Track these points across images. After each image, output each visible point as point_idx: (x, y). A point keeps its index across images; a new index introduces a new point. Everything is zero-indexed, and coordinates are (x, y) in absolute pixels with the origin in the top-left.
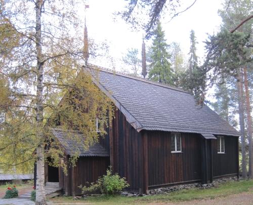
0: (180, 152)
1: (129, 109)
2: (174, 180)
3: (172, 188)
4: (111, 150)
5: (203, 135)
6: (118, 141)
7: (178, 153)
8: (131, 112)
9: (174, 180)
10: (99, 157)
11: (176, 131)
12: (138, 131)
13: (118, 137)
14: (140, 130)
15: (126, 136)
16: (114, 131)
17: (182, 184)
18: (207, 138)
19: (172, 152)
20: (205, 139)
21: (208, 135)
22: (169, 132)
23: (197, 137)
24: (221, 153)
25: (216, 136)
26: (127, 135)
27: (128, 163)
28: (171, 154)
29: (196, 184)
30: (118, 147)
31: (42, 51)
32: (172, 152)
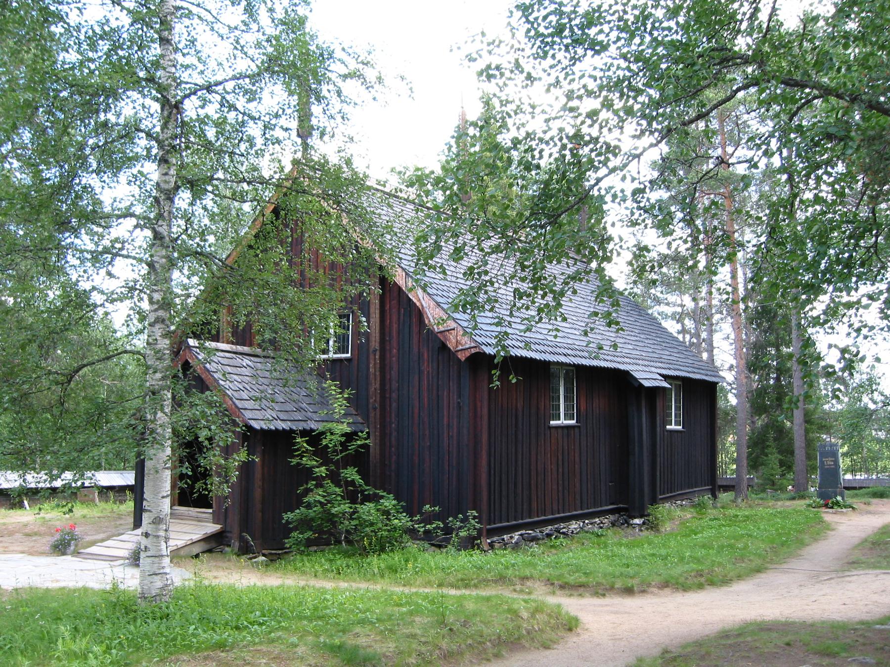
0: (573, 422)
1: (435, 292)
2: (555, 507)
3: (548, 529)
4: (372, 415)
5: (637, 375)
6: (395, 385)
7: (568, 427)
8: (439, 299)
9: (555, 507)
10: (269, 431)
11: (563, 359)
12: (462, 357)
13: (394, 374)
14: (468, 354)
15: (420, 372)
16: (383, 358)
17: (576, 518)
18: (646, 384)
19: (668, 427)
20: (641, 385)
21: (648, 375)
22: (546, 364)
23: (620, 381)
24: (563, 421)
25: (666, 377)
26: (424, 367)
27: (577, 459)
28: (550, 428)
29: (612, 518)
30: (394, 405)
31: (313, 119)
32: (668, 427)
